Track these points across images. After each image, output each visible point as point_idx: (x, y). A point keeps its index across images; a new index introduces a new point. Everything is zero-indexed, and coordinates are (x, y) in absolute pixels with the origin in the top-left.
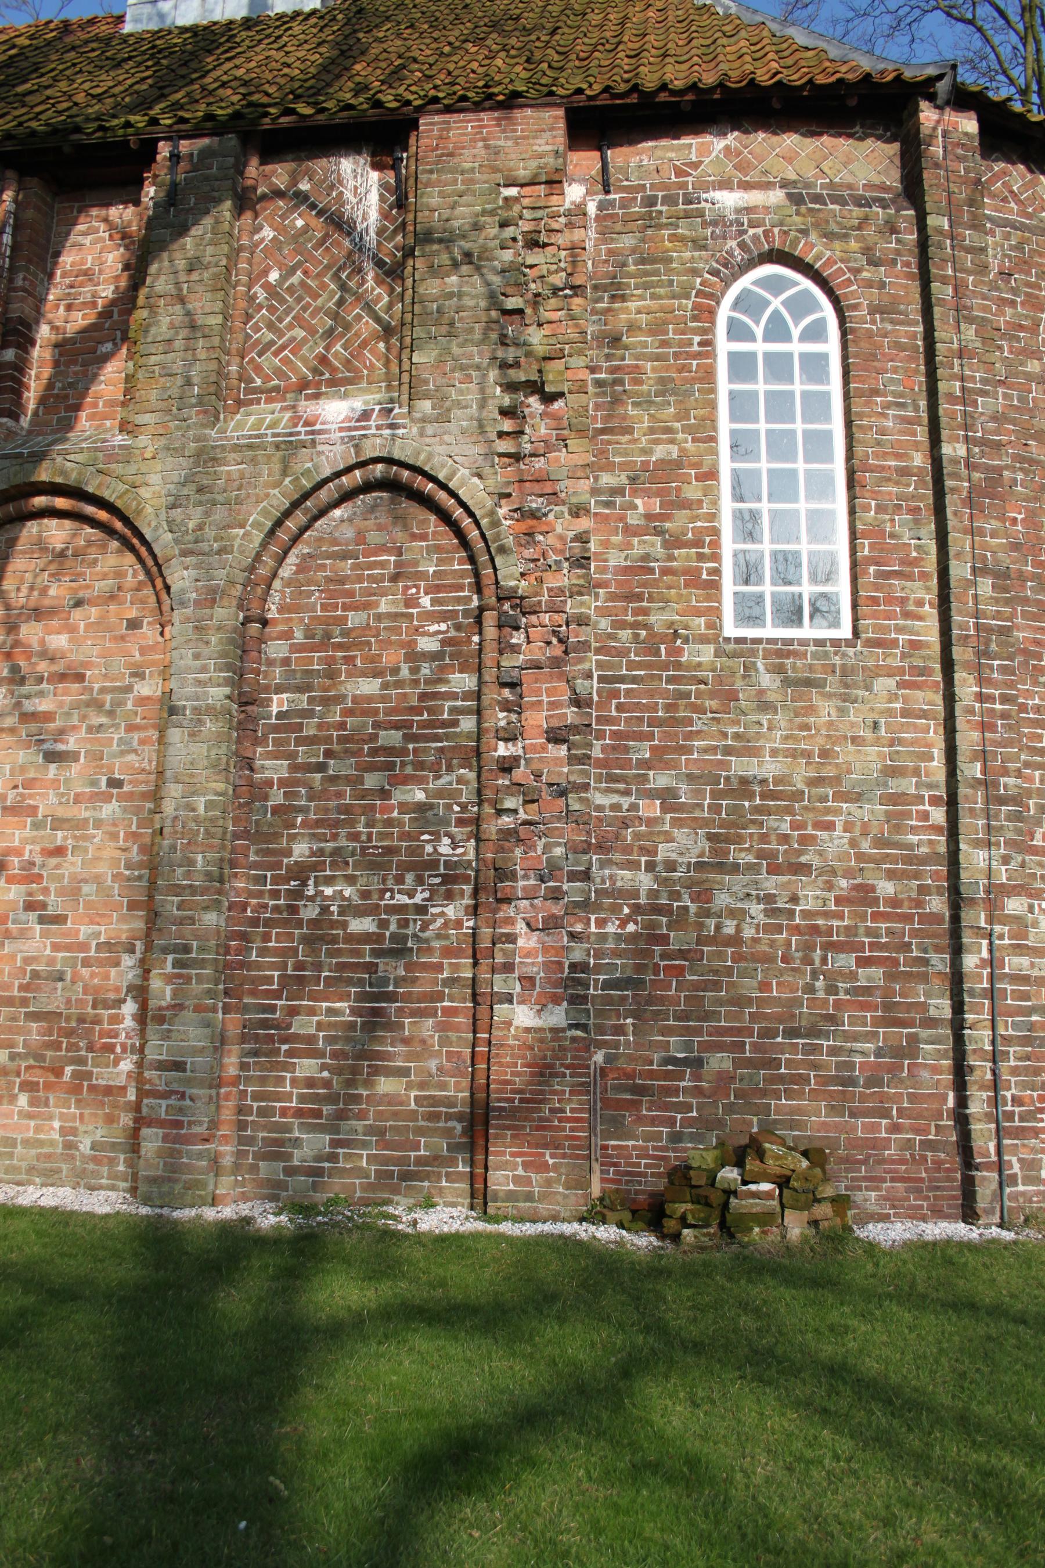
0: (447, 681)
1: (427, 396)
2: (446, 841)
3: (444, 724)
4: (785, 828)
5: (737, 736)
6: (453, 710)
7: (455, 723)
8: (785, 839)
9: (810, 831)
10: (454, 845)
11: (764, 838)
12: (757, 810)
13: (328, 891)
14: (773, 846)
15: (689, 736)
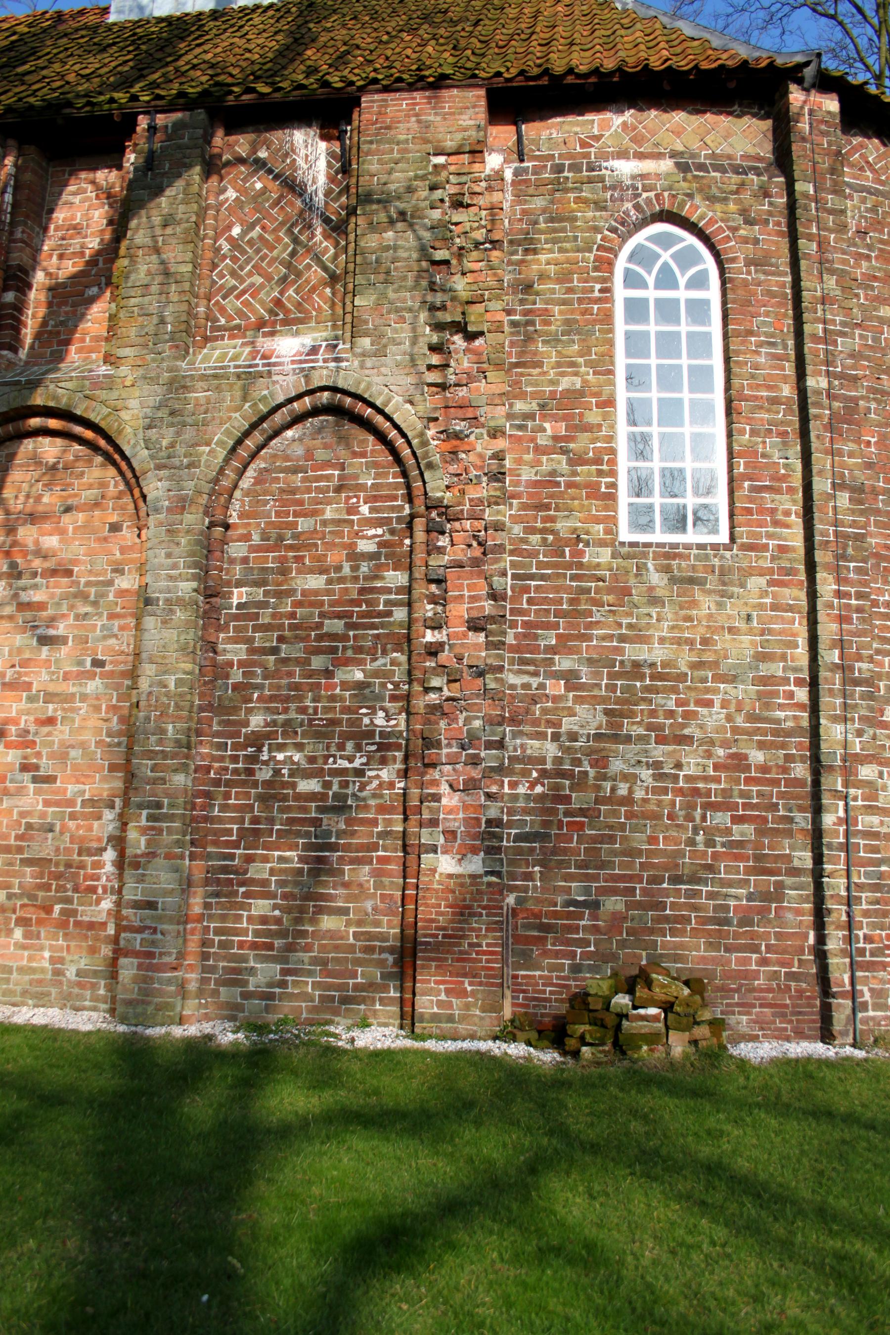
0: (383, 578)
1: (366, 334)
2: (381, 714)
3: (380, 614)
4: (671, 705)
5: (630, 626)
6: (388, 603)
7: (389, 614)
8: (671, 714)
9: (692, 707)
10: (388, 718)
11: (653, 713)
12: (647, 689)
13: (280, 757)
14: (661, 720)
15: (589, 626)
